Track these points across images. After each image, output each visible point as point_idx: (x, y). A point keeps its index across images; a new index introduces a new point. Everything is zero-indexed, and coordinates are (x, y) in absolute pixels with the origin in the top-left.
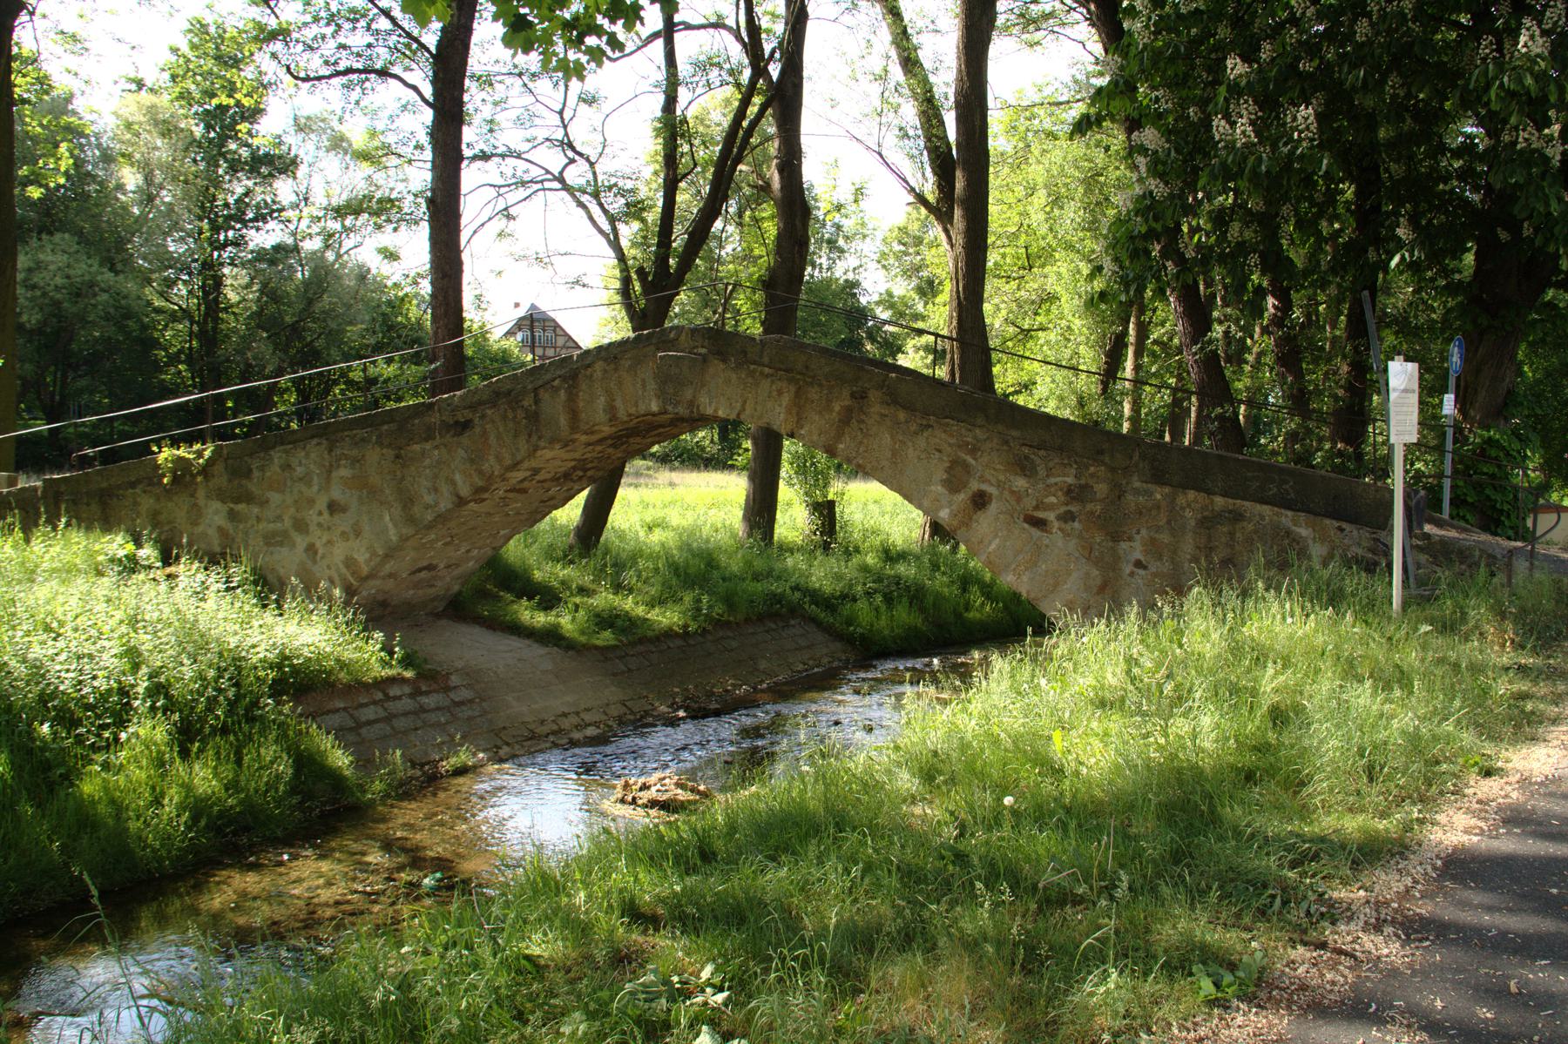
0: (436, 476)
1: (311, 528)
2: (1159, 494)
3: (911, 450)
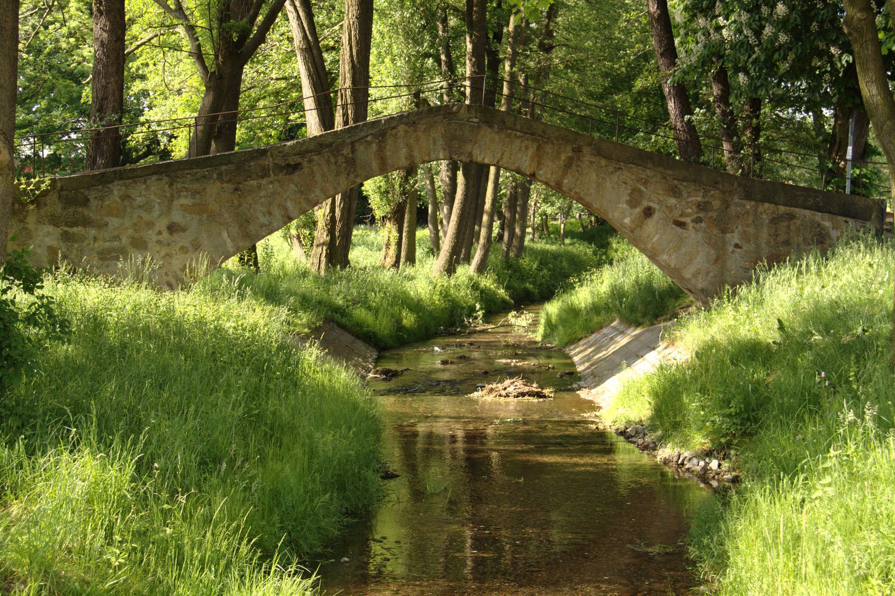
0: (270, 204)
1: (150, 245)
2: (749, 205)
3: (608, 184)
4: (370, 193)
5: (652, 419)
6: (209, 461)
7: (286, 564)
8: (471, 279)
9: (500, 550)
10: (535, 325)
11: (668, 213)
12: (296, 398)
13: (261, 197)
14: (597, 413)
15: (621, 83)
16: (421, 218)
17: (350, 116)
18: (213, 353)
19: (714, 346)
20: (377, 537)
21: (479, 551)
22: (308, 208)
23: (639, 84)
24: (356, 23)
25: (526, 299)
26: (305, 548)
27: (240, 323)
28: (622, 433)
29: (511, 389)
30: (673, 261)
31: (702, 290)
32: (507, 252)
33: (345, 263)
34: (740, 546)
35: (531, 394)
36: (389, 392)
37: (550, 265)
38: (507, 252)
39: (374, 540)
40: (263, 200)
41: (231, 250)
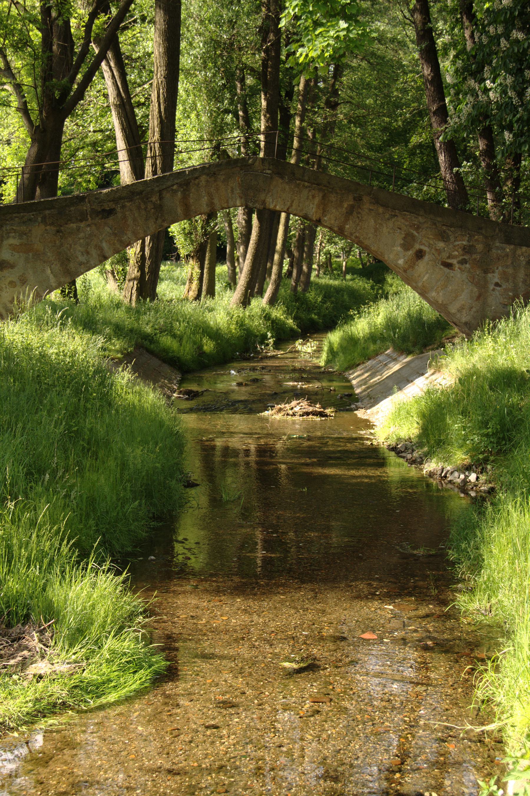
0: (88, 244)
3: (385, 229)
4: (176, 234)
5: (419, 436)
6: (34, 471)
7: (101, 562)
8: (263, 310)
9: (287, 551)
10: (319, 351)
11: (436, 255)
12: (110, 416)
13: (80, 239)
14: (372, 431)
15: (400, 136)
16: (220, 256)
17: (159, 166)
18: (38, 376)
19: (475, 373)
20: (180, 538)
21: (267, 552)
22: (121, 248)
23: (415, 140)
24: (164, 82)
25: (310, 329)
26: (117, 547)
27: (61, 350)
28: (393, 449)
29: (297, 409)
30: (440, 297)
31: (466, 324)
32: (296, 287)
33: (153, 295)
34: (494, 551)
35: (315, 413)
36: (191, 410)
37: (333, 299)
38: (296, 287)
39: (177, 541)
40: (82, 241)
41: (54, 285)
